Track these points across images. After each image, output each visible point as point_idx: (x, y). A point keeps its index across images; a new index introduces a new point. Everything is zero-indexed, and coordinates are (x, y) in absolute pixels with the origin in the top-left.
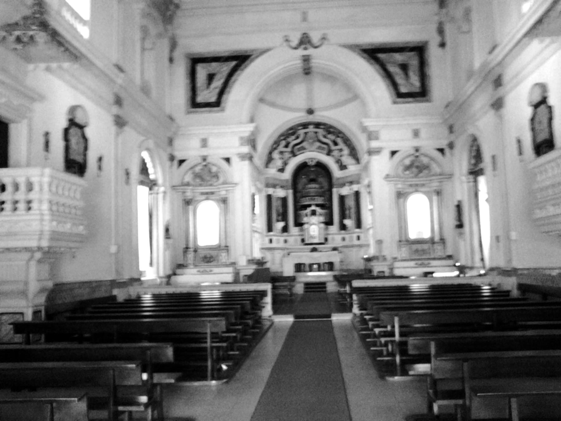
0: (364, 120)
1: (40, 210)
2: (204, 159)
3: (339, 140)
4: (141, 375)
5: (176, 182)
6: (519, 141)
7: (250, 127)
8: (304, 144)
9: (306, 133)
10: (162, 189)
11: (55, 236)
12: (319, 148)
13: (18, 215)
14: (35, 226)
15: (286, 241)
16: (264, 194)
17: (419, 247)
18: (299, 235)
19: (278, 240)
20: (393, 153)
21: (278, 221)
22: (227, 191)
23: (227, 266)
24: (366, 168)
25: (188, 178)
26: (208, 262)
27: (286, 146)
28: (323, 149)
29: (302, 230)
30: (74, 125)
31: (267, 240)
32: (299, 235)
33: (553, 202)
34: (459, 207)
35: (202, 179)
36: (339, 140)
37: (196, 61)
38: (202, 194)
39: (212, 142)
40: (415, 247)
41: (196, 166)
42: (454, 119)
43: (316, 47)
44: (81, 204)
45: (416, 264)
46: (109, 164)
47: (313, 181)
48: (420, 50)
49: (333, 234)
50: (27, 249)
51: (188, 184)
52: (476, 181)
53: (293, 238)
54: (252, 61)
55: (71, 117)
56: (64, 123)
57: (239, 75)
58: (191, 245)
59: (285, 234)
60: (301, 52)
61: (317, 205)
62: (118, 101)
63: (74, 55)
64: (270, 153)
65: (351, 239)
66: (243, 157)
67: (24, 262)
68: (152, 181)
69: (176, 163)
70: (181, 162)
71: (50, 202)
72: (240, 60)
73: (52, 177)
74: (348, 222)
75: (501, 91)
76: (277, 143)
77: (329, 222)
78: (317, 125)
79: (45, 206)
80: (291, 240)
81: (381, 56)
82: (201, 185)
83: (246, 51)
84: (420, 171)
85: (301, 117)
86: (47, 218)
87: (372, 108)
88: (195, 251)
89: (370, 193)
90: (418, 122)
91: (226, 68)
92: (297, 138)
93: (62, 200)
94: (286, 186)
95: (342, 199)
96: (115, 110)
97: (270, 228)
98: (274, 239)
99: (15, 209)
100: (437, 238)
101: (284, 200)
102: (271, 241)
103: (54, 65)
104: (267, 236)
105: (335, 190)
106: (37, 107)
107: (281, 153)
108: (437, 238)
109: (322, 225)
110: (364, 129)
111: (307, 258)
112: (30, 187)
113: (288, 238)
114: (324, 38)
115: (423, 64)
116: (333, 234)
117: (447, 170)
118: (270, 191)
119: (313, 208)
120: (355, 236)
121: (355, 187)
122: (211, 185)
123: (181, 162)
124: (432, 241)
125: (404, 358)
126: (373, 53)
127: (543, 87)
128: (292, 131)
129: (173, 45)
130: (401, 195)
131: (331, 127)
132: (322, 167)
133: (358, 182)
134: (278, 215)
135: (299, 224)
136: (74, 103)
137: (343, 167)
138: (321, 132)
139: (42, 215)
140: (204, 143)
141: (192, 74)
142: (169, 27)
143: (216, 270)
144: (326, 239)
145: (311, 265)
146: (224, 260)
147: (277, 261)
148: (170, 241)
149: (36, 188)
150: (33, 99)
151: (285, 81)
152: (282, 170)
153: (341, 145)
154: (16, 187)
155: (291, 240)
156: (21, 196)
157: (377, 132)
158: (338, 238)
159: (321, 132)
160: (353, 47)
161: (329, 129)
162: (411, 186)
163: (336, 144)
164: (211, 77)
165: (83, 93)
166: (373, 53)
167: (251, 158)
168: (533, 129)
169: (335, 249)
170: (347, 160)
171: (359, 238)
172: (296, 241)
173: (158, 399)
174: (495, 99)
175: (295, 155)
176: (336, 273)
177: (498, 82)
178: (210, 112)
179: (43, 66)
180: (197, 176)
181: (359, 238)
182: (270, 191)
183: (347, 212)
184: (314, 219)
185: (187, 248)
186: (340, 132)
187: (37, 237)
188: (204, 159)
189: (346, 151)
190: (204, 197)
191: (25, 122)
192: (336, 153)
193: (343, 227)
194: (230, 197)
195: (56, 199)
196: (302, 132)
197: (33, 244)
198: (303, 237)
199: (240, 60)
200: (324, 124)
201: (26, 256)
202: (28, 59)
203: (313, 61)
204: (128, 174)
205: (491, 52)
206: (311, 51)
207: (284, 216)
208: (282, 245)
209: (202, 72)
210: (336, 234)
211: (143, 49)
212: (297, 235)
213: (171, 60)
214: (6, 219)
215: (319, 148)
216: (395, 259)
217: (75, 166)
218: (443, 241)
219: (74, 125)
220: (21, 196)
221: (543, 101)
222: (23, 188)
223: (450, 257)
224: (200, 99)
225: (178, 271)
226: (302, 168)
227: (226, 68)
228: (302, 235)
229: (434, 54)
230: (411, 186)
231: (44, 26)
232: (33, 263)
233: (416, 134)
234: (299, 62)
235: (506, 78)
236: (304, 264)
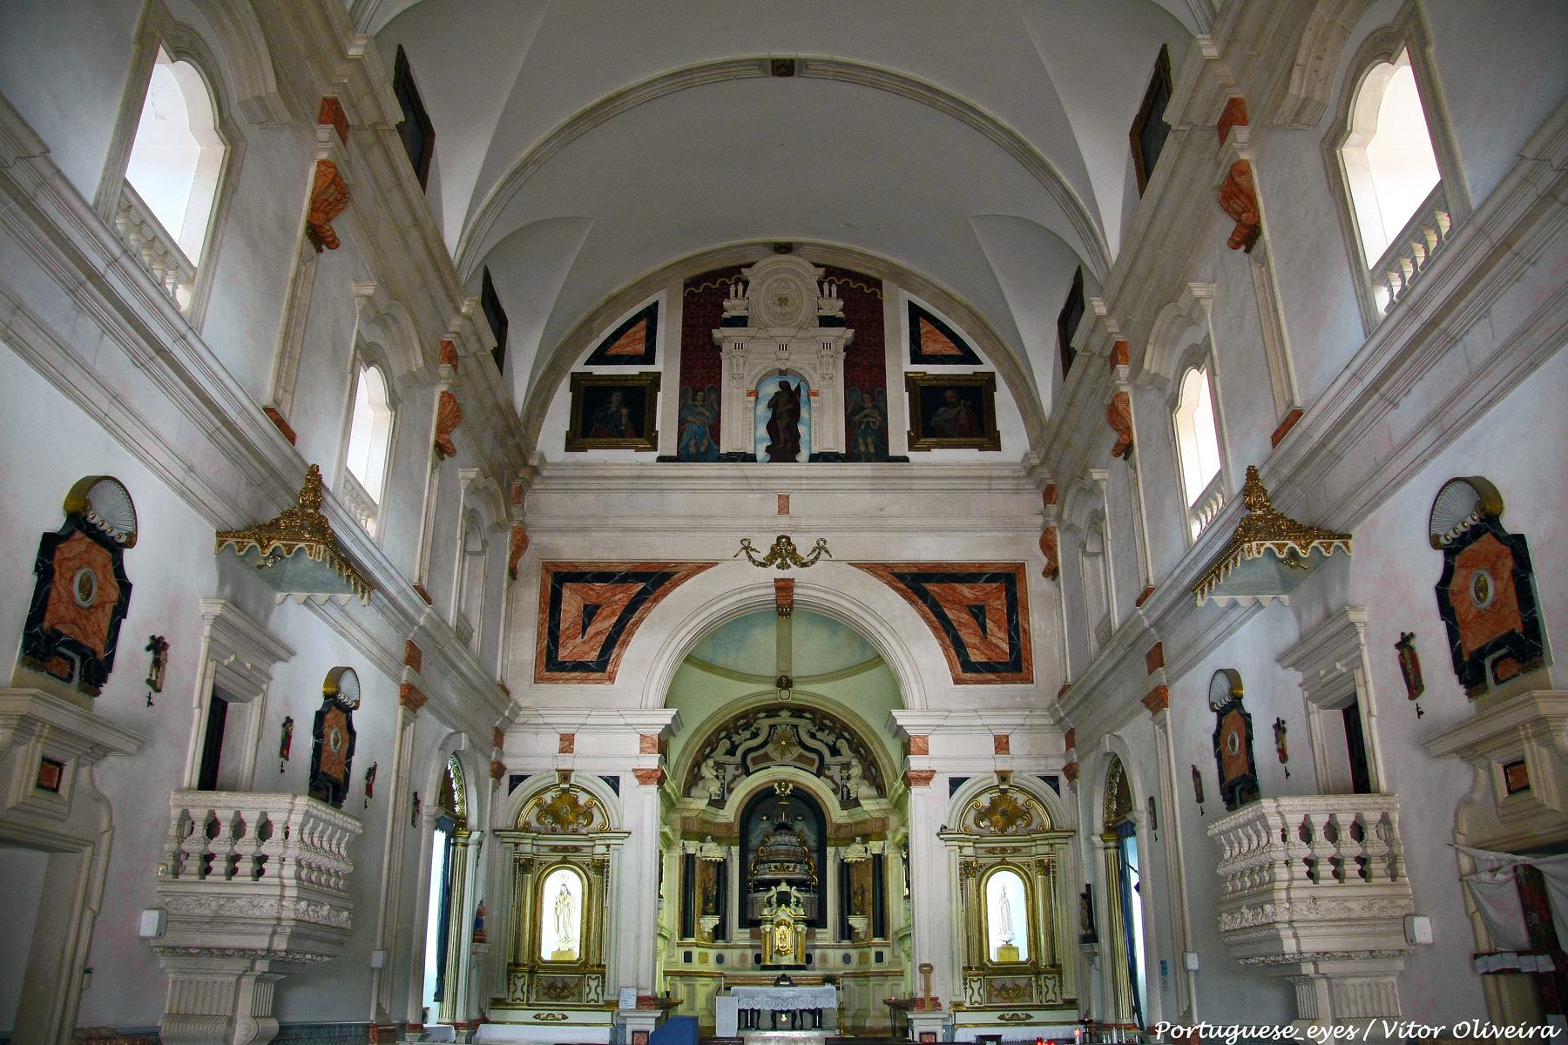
0: (895, 713)
1: (280, 877)
2: (565, 775)
3: (842, 745)
5: (504, 820)
6: (1196, 774)
7: (667, 717)
8: (769, 748)
9: (771, 726)
10: (475, 835)
11: (303, 931)
12: (800, 758)
13: (237, 885)
14: (268, 908)
15: (720, 959)
16: (677, 852)
17: (1007, 980)
18: (752, 947)
19: (705, 959)
20: (955, 783)
21: (705, 913)
22: (608, 846)
23: (597, 1008)
24: (900, 805)
25: (530, 814)
26: (558, 998)
27: (731, 752)
28: (811, 762)
29: (756, 936)
30: (336, 707)
31: (680, 953)
32: (752, 947)
33: (1252, 901)
34: (1087, 897)
35: (557, 818)
36: (842, 745)
37: (561, 577)
38: (555, 849)
39: (582, 742)
40: (999, 980)
41: (547, 789)
42: (1075, 717)
43: (804, 565)
44: (346, 868)
45: (1001, 1017)
46: (386, 783)
47: (783, 828)
48: (1009, 579)
49: (822, 947)
50: (243, 952)
51: (527, 828)
52: (1121, 847)
53: (737, 952)
54: (676, 585)
55: (332, 690)
56: (318, 702)
57: (648, 610)
58: (524, 958)
59: (720, 942)
60: (774, 572)
61: (790, 883)
62: (413, 658)
63: (364, 582)
64: (697, 764)
65: (863, 959)
66: (644, 777)
67: (233, 979)
68: (457, 818)
69: (505, 780)
70: (516, 780)
71: (298, 862)
72: (654, 580)
73: (307, 814)
75: (1162, 675)
76: (711, 744)
77: (816, 921)
78: (798, 711)
79: (289, 871)
80: (732, 956)
81: (931, 587)
82: (554, 831)
83: (666, 565)
84: (1011, 822)
85: (760, 692)
86: (291, 892)
87: (913, 692)
88: (532, 972)
89: (906, 861)
90: (1003, 722)
91: (622, 596)
92: (755, 735)
93: (318, 860)
94: (730, 838)
95: (845, 868)
96: (405, 674)
97: (687, 929)
98: (696, 952)
99: (208, 871)
100: (1044, 962)
101: (721, 867)
102: (688, 957)
103: (321, 597)
104: (679, 945)
105: (830, 851)
106: (278, 669)
107: (719, 766)
108: (1044, 962)
109: (801, 927)
110: (899, 731)
111: (765, 998)
112: (264, 831)
113: (726, 953)
114: (820, 548)
115: (1015, 606)
116: (822, 947)
117: (1065, 822)
118: (692, 847)
119: (784, 887)
120: (872, 952)
121: (875, 847)
122: (575, 832)
123: (516, 780)
124: (1031, 968)
126: (918, 583)
127: (1233, 677)
128: (744, 720)
129: (521, 544)
130: (973, 872)
131: (826, 716)
132: (806, 802)
133: (882, 837)
135: (750, 922)
136: (336, 662)
137: (849, 802)
138: (804, 725)
139: (283, 886)
140: (567, 744)
141: (553, 604)
142: (514, 510)
143: (573, 1016)
144: (809, 958)
145: (774, 1014)
146: (593, 996)
147: (701, 1002)
148: (483, 948)
149: (277, 832)
150: (276, 658)
151: (736, 623)
152: (719, 803)
153: (846, 754)
154: (239, 829)
155: (732, 956)
156: (247, 846)
157: (925, 739)
158: (835, 956)
159: (804, 725)
160: (875, 569)
161: (822, 720)
162: (991, 851)
163: (835, 751)
164: (590, 612)
165: (356, 644)
166: (918, 583)
167: (661, 781)
168: (1219, 756)
169: (829, 979)
170: (863, 790)
171: (879, 957)
172: (743, 958)
173: (1313, 707)
174: (1151, 688)
175: (748, 773)
176: (830, 1034)
177: (1156, 658)
178: (582, 681)
179: (303, 595)
180: (546, 811)
181: (879, 957)
182: (692, 847)
183: (857, 900)
184: (784, 913)
185: (516, 964)
186: (845, 727)
187: (270, 930)
188: (565, 775)
189: (856, 770)
190: (558, 857)
191: (258, 700)
192: (835, 771)
193: (846, 932)
194: (613, 858)
195: (307, 856)
196: (764, 724)
197: (261, 943)
199: (654, 580)
200: (813, 711)
201: (240, 965)
202: (277, 583)
203: (796, 590)
204: (417, 802)
205: (1139, 603)
206: (793, 572)
207: (718, 905)
208: (711, 966)
209: (572, 603)
210: (832, 947)
211: (465, 552)
213: (513, 573)
214: (216, 889)
215: (800, 758)
216: (957, 1006)
217: (328, 785)
218: (1056, 968)
219: (336, 707)
220: (247, 846)
221: (1236, 702)
222: (225, 830)
223: (1071, 1004)
224: (563, 654)
225: (494, 1015)
226: (761, 801)
227: (622, 596)
228: (758, 947)
229: (1035, 584)
230: (991, 851)
231: (321, 531)
232: (248, 982)
233: (1002, 745)
234: (773, 590)
235: (1170, 652)
236: (759, 1011)
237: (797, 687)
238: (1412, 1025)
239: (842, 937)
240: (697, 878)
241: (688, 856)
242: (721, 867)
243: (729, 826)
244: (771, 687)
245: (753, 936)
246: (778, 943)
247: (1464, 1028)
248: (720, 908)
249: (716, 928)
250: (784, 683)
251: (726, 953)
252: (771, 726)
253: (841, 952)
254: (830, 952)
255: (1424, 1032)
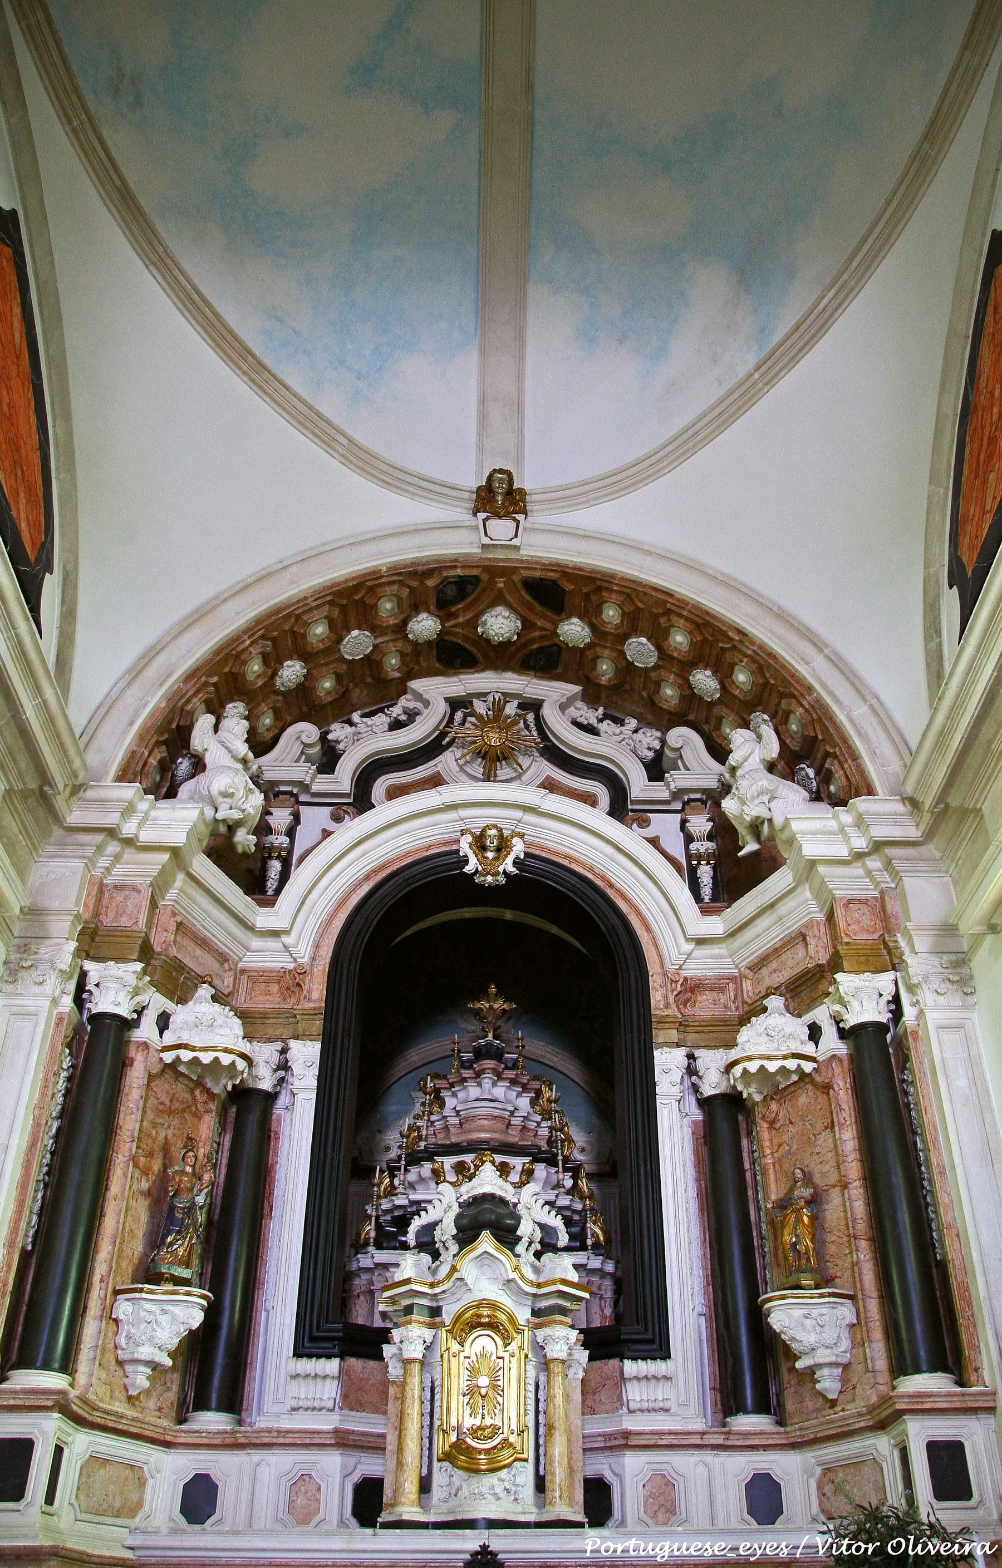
4: (618, 1317)
8: (446, 762)
9: (455, 704)
15: (199, 1499)
21: (149, 1274)
32: (344, 1441)
53: (277, 1465)
59: (212, 1421)
74: (810, 1324)
77: (626, 1329)
95: (725, 1117)
113: (226, 1468)
118: (117, 988)
125: (403, 1239)
134: (165, 1217)
135: (341, 1328)
172: (300, 1504)
184: (484, 1275)
193: (752, 1370)
198: (370, 1466)
212: (308, 1442)
228: (374, 1445)
237: (538, 516)
238: (846, 1542)
239: (729, 1401)
240: (130, 1121)
241: (98, 1019)
242: (249, 1111)
243: (292, 981)
244: (461, 514)
245: (353, 1397)
246: (460, 1414)
247: (899, 1544)
248: (227, 1247)
249: (197, 1347)
250: (500, 497)
251: (226, 1468)
252: (455, 704)
253: (740, 1466)
254: (686, 1465)
255: (858, 1548)
